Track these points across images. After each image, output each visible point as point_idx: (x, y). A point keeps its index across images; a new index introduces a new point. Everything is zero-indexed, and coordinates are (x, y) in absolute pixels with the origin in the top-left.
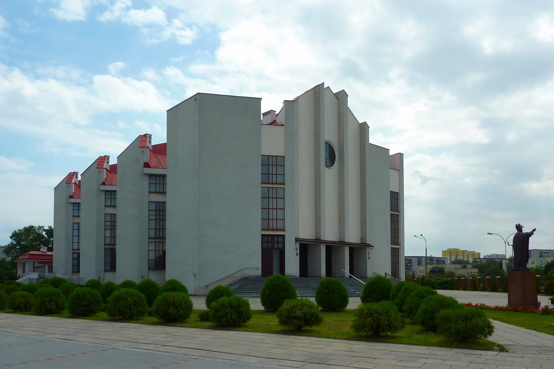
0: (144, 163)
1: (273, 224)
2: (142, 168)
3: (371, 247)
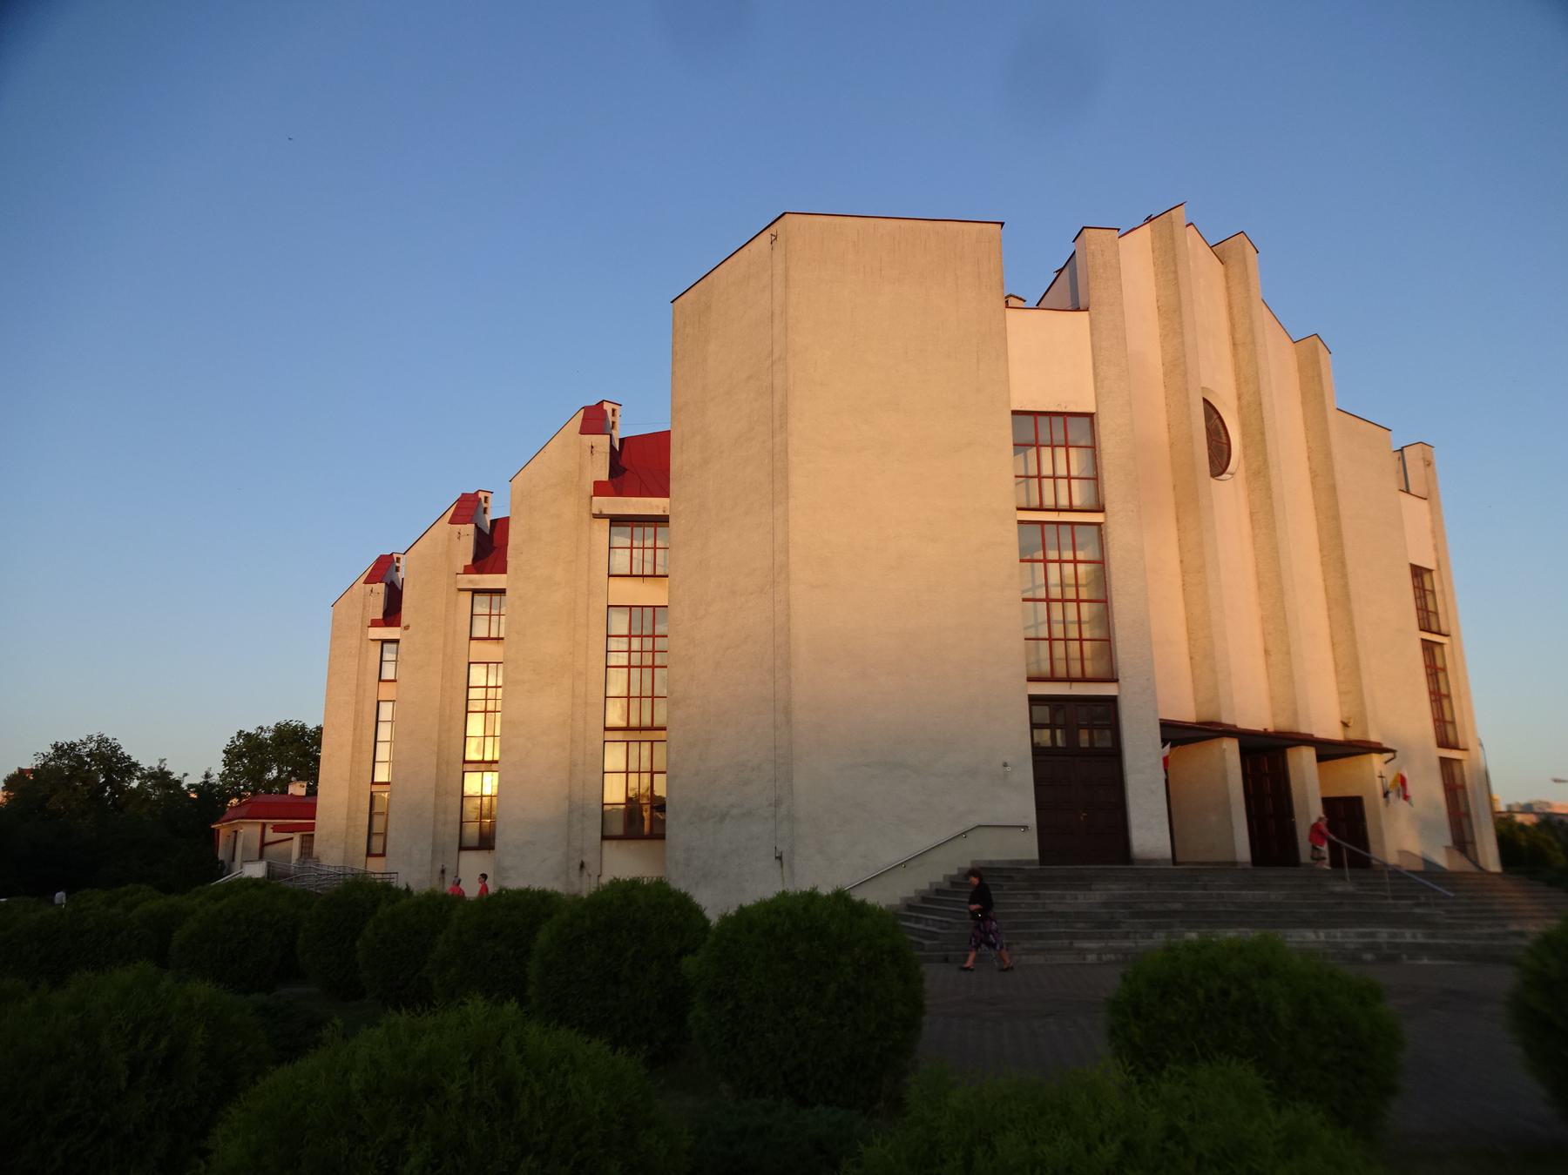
0: (595, 482)
1: (308, 838)
2: (587, 500)
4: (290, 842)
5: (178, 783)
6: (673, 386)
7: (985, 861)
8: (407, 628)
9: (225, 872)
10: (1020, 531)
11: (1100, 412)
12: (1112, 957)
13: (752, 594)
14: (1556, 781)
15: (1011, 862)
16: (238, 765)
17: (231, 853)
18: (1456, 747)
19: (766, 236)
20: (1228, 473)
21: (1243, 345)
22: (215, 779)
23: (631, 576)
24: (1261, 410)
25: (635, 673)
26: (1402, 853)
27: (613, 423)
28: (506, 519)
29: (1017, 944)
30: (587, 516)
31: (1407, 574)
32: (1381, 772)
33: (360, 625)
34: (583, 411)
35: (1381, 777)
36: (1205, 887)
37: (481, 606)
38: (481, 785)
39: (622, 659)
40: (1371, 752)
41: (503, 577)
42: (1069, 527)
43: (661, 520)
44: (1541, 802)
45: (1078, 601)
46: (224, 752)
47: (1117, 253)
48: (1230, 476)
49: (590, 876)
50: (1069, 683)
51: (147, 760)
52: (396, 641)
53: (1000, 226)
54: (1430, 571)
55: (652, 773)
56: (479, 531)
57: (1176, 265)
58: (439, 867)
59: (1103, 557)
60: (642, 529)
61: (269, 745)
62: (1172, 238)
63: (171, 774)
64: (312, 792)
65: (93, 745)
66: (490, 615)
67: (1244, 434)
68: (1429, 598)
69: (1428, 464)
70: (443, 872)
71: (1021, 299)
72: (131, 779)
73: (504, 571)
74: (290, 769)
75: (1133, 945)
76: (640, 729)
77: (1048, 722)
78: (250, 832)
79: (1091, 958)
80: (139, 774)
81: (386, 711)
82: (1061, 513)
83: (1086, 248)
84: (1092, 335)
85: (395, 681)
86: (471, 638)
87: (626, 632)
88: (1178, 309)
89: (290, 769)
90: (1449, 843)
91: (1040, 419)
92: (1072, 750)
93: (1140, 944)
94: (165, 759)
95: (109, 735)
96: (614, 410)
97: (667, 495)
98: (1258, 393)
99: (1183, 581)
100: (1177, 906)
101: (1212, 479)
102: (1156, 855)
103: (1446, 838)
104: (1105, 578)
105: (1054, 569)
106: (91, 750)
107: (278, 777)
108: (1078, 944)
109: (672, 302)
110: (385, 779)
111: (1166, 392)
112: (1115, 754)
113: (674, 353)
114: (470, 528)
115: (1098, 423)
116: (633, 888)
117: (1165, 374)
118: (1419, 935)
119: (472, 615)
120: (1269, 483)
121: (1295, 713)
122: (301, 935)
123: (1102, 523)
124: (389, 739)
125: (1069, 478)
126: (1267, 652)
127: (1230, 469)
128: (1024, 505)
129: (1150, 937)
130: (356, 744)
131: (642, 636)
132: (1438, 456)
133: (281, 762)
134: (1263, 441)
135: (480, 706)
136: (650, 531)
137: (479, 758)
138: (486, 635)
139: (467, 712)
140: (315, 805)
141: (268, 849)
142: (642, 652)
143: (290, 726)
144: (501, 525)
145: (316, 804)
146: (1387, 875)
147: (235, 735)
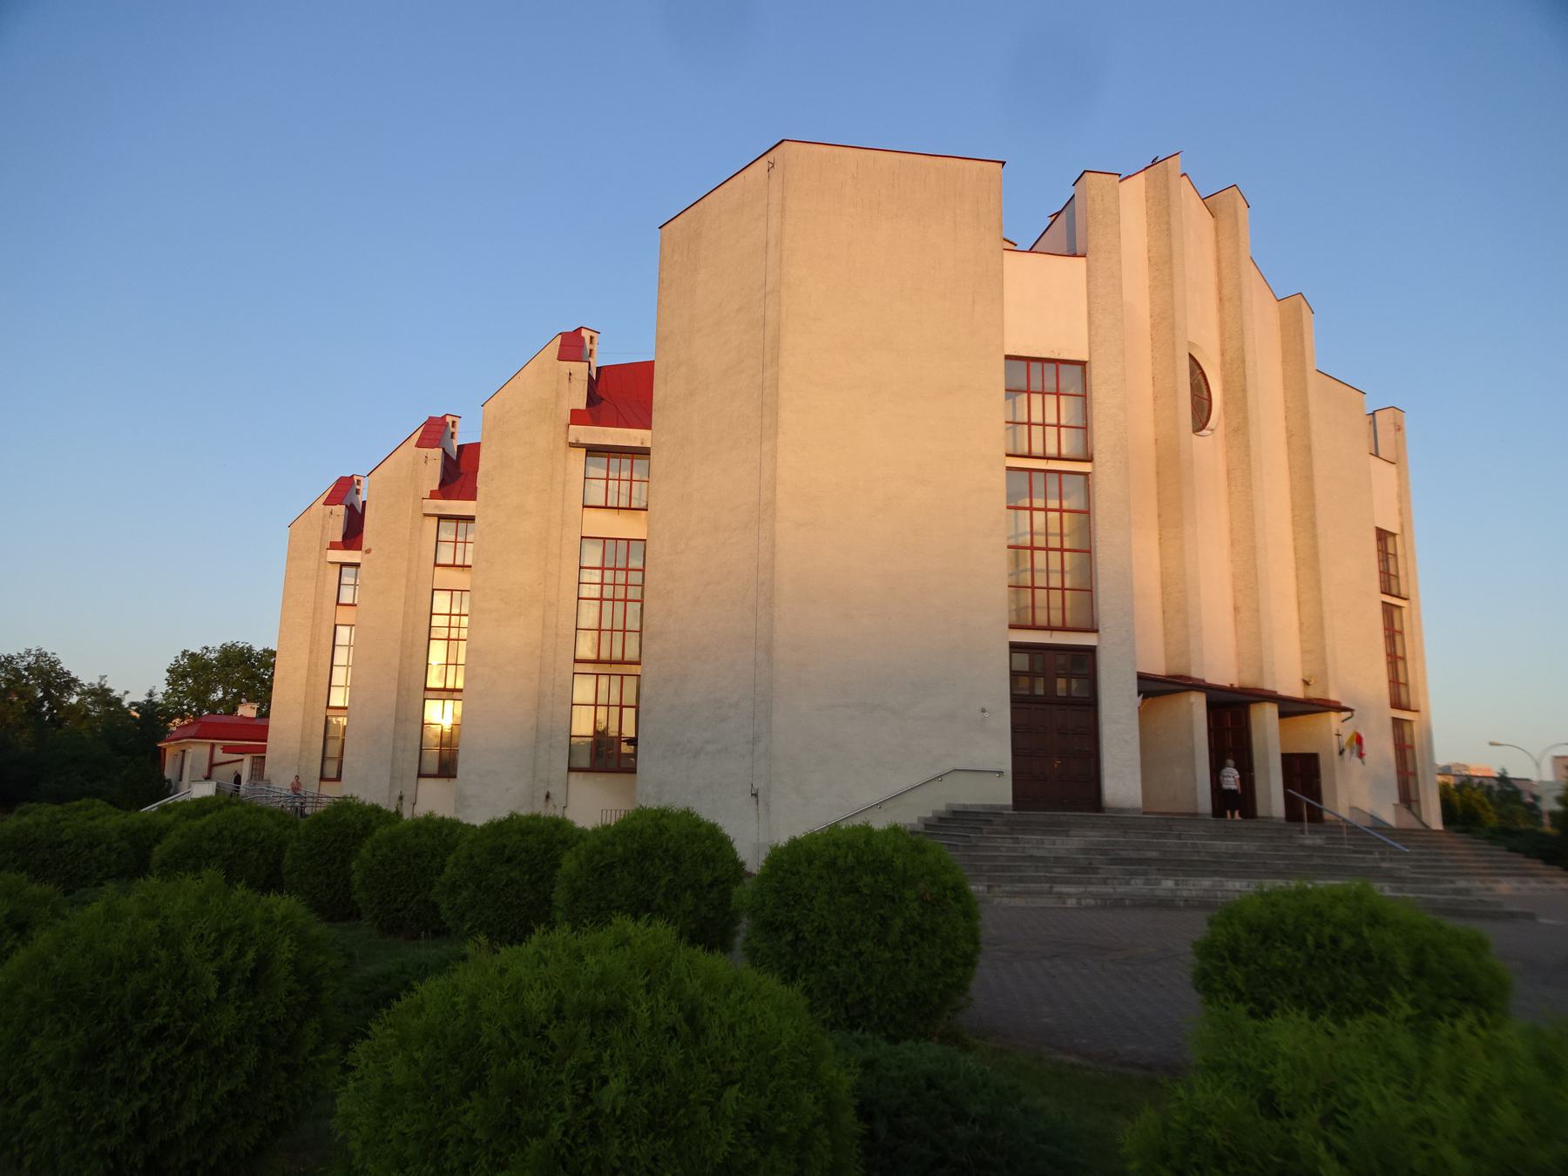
1: (259, 760)
2: (563, 429)
3: (1343, 713)
4: (239, 763)
5: (119, 700)
6: (659, 315)
7: (960, 805)
8: (368, 551)
9: (171, 792)
10: (1007, 476)
11: (1092, 361)
12: (1092, 902)
13: (735, 530)
14: (1492, 744)
15: (984, 806)
16: (182, 685)
17: (179, 774)
18: (1407, 709)
19: (763, 162)
20: (1208, 430)
21: (1229, 300)
22: (158, 698)
23: (606, 507)
24: (1244, 367)
25: (607, 605)
26: (1353, 809)
27: (591, 350)
28: (476, 446)
29: (999, 886)
30: (562, 445)
31: (1373, 537)
32: (1338, 730)
33: (318, 548)
34: (560, 336)
35: (1338, 735)
36: (1179, 837)
37: (446, 532)
38: (441, 716)
39: (594, 591)
40: (1328, 711)
41: (472, 503)
42: (1057, 475)
43: (643, 452)
44: (1458, 765)
45: (1062, 550)
46: (168, 671)
47: (1117, 198)
48: (1209, 432)
49: (555, 806)
50: (1049, 632)
51: (87, 676)
52: (357, 565)
53: (1001, 165)
54: (1394, 535)
55: (621, 707)
56: (446, 456)
57: (1169, 215)
58: (398, 794)
59: (1089, 508)
60: (618, 460)
61: (214, 666)
62: (1167, 188)
63: (111, 691)
64: (264, 715)
65: (31, 659)
66: (456, 542)
67: (1225, 391)
68: (1391, 562)
69: (1399, 429)
70: (401, 798)
71: (1012, 243)
72: (70, 695)
73: (474, 498)
74: (235, 690)
75: (1111, 890)
76: (611, 662)
77: (1027, 669)
78: (198, 752)
79: (1071, 902)
80: (78, 690)
81: (344, 634)
82: (1050, 461)
83: (1086, 193)
84: (1088, 282)
85: (353, 605)
86: (436, 565)
87: (598, 564)
88: (1169, 260)
89: (235, 690)
90: (1397, 801)
91: (1047, 366)
92: (1050, 700)
93: (1118, 890)
94: (106, 676)
95: (48, 650)
96: (591, 338)
97: (648, 427)
98: (1242, 349)
99: (1160, 534)
100: (1154, 854)
101: (1194, 435)
102: (1127, 804)
103: (1394, 796)
104: (1090, 528)
105: (1039, 517)
106: (29, 664)
107: (224, 697)
108: (1058, 888)
109: (660, 228)
110: (341, 704)
111: (1152, 345)
112: (1090, 704)
113: (661, 281)
114: (438, 452)
115: (1091, 372)
116: (663, 815)
117: (1153, 326)
118: (1387, 888)
119: (437, 541)
120: (1248, 441)
121: (1261, 669)
122: (287, 855)
123: (1089, 473)
124: (346, 664)
125: (1059, 426)
126: (1236, 609)
127: (1210, 425)
128: (1011, 452)
129: (1128, 884)
130: (312, 668)
131: (615, 569)
132: (1408, 422)
133: (227, 684)
134: (1244, 397)
135: (444, 633)
136: (626, 462)
137: (441, 685)
138: (452, 563)
139: (430, 639)
140: (266, 728)
141: (217, 770)
142: (614, 585)
143: (237, 647)
144: (470, 453)
145: (268, 726)
146: (1345, 831)
147: (180, 654)
